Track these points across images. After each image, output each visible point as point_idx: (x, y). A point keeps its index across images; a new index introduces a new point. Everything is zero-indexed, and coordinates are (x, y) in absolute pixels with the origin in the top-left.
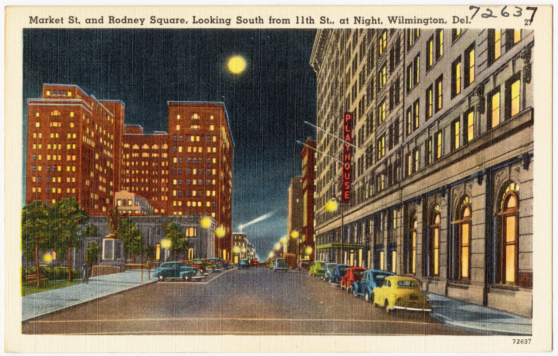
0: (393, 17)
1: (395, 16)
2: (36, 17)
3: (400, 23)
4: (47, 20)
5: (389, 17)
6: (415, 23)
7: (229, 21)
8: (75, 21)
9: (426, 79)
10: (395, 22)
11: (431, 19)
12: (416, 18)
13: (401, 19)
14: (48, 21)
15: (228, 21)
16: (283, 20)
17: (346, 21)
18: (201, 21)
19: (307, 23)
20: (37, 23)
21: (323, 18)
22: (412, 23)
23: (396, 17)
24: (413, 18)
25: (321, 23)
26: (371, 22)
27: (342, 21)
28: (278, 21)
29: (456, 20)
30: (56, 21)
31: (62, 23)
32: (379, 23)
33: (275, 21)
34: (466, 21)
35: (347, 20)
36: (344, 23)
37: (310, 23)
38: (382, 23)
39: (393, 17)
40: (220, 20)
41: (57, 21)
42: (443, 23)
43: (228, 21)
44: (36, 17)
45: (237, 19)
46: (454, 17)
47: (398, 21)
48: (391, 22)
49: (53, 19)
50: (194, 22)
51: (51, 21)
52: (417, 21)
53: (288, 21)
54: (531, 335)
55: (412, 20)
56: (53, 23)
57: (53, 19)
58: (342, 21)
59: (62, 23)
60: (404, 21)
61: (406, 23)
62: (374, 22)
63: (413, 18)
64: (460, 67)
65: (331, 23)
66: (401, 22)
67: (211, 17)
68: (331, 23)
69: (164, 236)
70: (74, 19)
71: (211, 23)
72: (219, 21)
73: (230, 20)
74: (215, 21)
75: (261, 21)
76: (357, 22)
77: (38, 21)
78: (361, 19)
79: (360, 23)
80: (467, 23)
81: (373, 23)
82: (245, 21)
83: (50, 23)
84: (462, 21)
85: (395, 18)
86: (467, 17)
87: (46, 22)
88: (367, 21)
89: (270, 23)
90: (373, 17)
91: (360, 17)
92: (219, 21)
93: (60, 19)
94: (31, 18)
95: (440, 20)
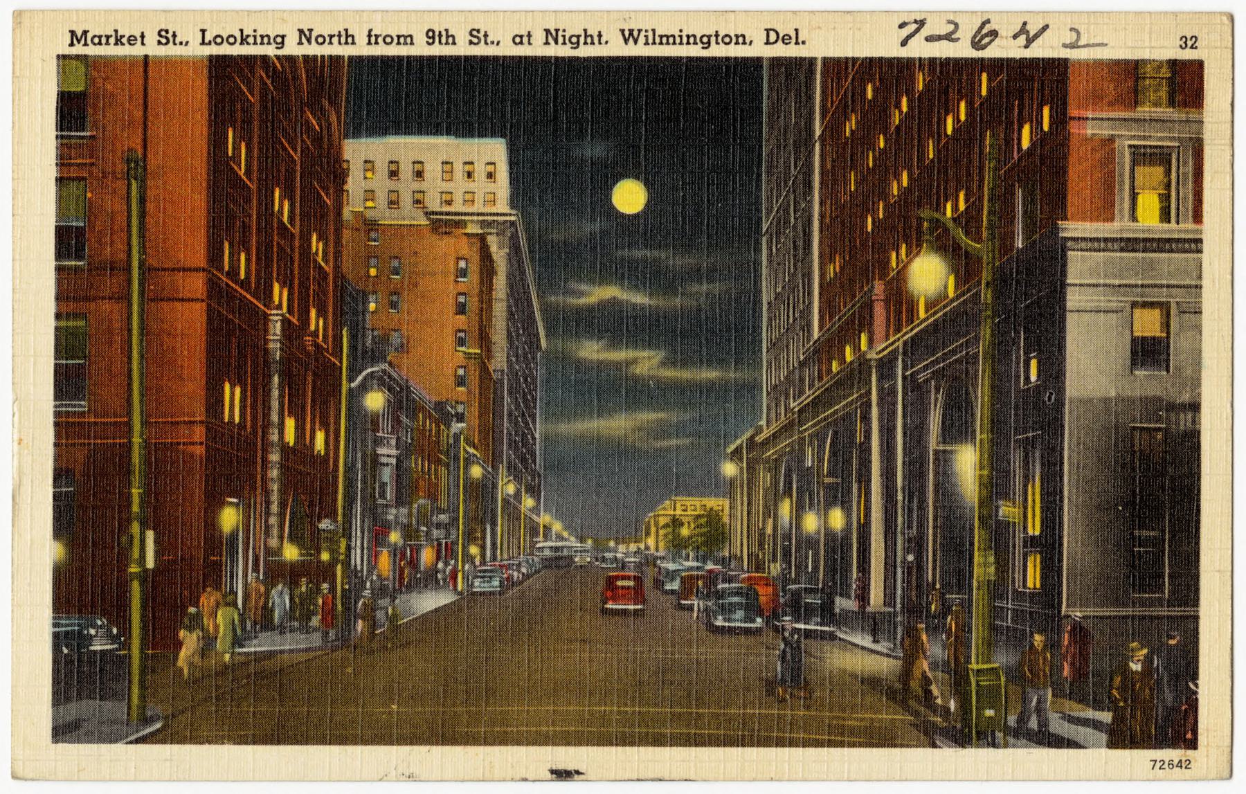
0: (631, 31)
1: (635, 27)
3: (647, 43)
4: (108, 37)
5: (623, 31)
6: (681, 43)
7: (281, 41)
10: (636, 42)
11: (717, 35)
13: (650, 34)
14: (112, 40)
15: (279, 40)
16: (399, 37)
17: (525, 40)
18: (219, 40)
20: (86, 44)
22: (674, 43)
23: (640, 31)
24: (677, 34)
25: (471, 43)
26: (582, 40)
27: (518, 40)
28: (388, 40)
29: (773, 37)
30: (129, 40)
31: (143, 44)
32: (486, 43)
33: (380, 40)
34: (794, 40)
35: (529, 35)
36: (521, 43)
37: (346, 43)
38: (751, 42)
39: (631, 31)
40: (262, 37)
41: (131, 40)
42: (744, 43)
43: (279, 40)
44: (85, 32)
46: (768, 30)
48: (626, 41)
50: (203, 43)
51: (117, 40)
53: (409, 40)
55: (673, 36)
56: (123, 44)
58: (518, 40)
59: (143, 44)
60: (658, 40)
61: (661, 43)
62: (589, 40)
63: (677, 34)
65: (493, 43)
66: (650, 41)
67: (242, 31)
68: (493, 43)
69: (718, 474)
70: (481, 35)
71: (241, 43)
73: (283, 37)
74: (251, 40)
75: (348, 38)
76: (550, 40)
77: (89, 42)
78: (560, 33)
79: (556, 43)
80: (797, 43)
81: (585, 43)
82: (388, 40)
83: (116, 44)
84: (786, 40)
85: (635, 33)
86: (796, 30)
88: (574, 40)
89: (369, 43)
90: (585, 31)
91: (557, 31)
93: (138, 35)
94: (73, 33)
95: (737, 36)
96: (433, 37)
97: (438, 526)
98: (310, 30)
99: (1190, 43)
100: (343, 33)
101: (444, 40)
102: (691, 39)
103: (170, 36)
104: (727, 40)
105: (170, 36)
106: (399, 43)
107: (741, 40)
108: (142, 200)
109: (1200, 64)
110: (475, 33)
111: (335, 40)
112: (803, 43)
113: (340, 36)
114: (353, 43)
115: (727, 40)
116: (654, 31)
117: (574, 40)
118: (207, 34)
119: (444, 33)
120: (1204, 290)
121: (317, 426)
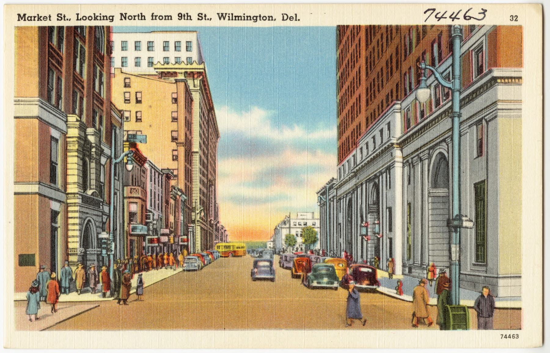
1: (224, 13)
2: (25, 15)
3: (229, 20)
4: (35, 17)
5: (218, 14)
6: (244, 20)
8: (204, 18)
9: (416, 52)
11: (260, 16)
12: (102, 16)
13: (231, 16)
14: (36, 19)
16: (165, 16)
18: (84, 18)
19: (139, 19)
21: (200, 15)
22: (241, 20)
23: (226, 14)
24: (242, 15)
29: (285, 17)
31: (50, 20)
37: (142, 19)
39: (222, 14)
40: (104, 17)
41: (45, 18)
42: (272, 20)
43: (111, 18)
44: (25, 15)
45: (198, 15)
47: (227, 18)
48: (220, 19)
49: (41, 17)
50: (78, 20)
51: (38, 18)
52: (246, 18)
53: (170, 18)
54: (16, 194)
55: (241, 17)
56: (97, 20)
57: (41, 17)
59: (50, 20)
60: (234, 18)
61: (235, 20)
63: (242, 15)
64: (436, 46)
65: (67, 20)
66: (231, 18)
67: (94, 14)
68: (208, 19)
70: (203, 16)
71: (95, 20)
72: (102, 18)
73: (113, 17)
76: (123, 18)
77: (26, 19)
80: (296, 20)
83: (38, 20)
84: (291, 18)
85: (224, 15)
86: (296, 15)
87: (34, 20)
89: (152, 19)
92: (102, 18)
93: (48, 16)
94: (19, 15)
96: (181, 17)
97: (163, 235)
98: (126, 14)
99: (514, 19)
100: (140, 15)
101: (140, 18)
102: (249, 18)
103: (62, 16)
104: (264, 18)
105: (62, 16)
106: (165, 19)
107: (271, 18)
108: (390, 178)
109: (520, 27)
110: (200, 15)
111: (136, 18)
112: (299, 20)
113: (138, 16)
114: (145, 19)
115: (264, 18)
116: (232, 14)
117: (255, 18)
118: (79, 16)
119: (186, 15)
120: (523, 118)
121: (263, 259)
